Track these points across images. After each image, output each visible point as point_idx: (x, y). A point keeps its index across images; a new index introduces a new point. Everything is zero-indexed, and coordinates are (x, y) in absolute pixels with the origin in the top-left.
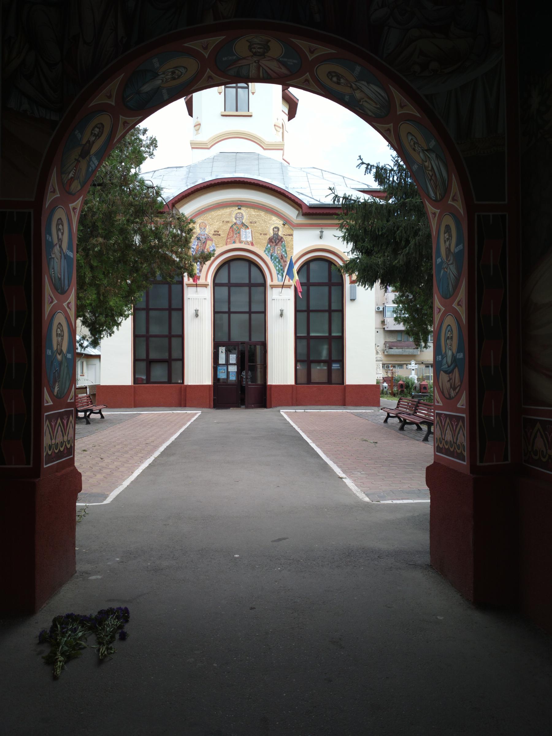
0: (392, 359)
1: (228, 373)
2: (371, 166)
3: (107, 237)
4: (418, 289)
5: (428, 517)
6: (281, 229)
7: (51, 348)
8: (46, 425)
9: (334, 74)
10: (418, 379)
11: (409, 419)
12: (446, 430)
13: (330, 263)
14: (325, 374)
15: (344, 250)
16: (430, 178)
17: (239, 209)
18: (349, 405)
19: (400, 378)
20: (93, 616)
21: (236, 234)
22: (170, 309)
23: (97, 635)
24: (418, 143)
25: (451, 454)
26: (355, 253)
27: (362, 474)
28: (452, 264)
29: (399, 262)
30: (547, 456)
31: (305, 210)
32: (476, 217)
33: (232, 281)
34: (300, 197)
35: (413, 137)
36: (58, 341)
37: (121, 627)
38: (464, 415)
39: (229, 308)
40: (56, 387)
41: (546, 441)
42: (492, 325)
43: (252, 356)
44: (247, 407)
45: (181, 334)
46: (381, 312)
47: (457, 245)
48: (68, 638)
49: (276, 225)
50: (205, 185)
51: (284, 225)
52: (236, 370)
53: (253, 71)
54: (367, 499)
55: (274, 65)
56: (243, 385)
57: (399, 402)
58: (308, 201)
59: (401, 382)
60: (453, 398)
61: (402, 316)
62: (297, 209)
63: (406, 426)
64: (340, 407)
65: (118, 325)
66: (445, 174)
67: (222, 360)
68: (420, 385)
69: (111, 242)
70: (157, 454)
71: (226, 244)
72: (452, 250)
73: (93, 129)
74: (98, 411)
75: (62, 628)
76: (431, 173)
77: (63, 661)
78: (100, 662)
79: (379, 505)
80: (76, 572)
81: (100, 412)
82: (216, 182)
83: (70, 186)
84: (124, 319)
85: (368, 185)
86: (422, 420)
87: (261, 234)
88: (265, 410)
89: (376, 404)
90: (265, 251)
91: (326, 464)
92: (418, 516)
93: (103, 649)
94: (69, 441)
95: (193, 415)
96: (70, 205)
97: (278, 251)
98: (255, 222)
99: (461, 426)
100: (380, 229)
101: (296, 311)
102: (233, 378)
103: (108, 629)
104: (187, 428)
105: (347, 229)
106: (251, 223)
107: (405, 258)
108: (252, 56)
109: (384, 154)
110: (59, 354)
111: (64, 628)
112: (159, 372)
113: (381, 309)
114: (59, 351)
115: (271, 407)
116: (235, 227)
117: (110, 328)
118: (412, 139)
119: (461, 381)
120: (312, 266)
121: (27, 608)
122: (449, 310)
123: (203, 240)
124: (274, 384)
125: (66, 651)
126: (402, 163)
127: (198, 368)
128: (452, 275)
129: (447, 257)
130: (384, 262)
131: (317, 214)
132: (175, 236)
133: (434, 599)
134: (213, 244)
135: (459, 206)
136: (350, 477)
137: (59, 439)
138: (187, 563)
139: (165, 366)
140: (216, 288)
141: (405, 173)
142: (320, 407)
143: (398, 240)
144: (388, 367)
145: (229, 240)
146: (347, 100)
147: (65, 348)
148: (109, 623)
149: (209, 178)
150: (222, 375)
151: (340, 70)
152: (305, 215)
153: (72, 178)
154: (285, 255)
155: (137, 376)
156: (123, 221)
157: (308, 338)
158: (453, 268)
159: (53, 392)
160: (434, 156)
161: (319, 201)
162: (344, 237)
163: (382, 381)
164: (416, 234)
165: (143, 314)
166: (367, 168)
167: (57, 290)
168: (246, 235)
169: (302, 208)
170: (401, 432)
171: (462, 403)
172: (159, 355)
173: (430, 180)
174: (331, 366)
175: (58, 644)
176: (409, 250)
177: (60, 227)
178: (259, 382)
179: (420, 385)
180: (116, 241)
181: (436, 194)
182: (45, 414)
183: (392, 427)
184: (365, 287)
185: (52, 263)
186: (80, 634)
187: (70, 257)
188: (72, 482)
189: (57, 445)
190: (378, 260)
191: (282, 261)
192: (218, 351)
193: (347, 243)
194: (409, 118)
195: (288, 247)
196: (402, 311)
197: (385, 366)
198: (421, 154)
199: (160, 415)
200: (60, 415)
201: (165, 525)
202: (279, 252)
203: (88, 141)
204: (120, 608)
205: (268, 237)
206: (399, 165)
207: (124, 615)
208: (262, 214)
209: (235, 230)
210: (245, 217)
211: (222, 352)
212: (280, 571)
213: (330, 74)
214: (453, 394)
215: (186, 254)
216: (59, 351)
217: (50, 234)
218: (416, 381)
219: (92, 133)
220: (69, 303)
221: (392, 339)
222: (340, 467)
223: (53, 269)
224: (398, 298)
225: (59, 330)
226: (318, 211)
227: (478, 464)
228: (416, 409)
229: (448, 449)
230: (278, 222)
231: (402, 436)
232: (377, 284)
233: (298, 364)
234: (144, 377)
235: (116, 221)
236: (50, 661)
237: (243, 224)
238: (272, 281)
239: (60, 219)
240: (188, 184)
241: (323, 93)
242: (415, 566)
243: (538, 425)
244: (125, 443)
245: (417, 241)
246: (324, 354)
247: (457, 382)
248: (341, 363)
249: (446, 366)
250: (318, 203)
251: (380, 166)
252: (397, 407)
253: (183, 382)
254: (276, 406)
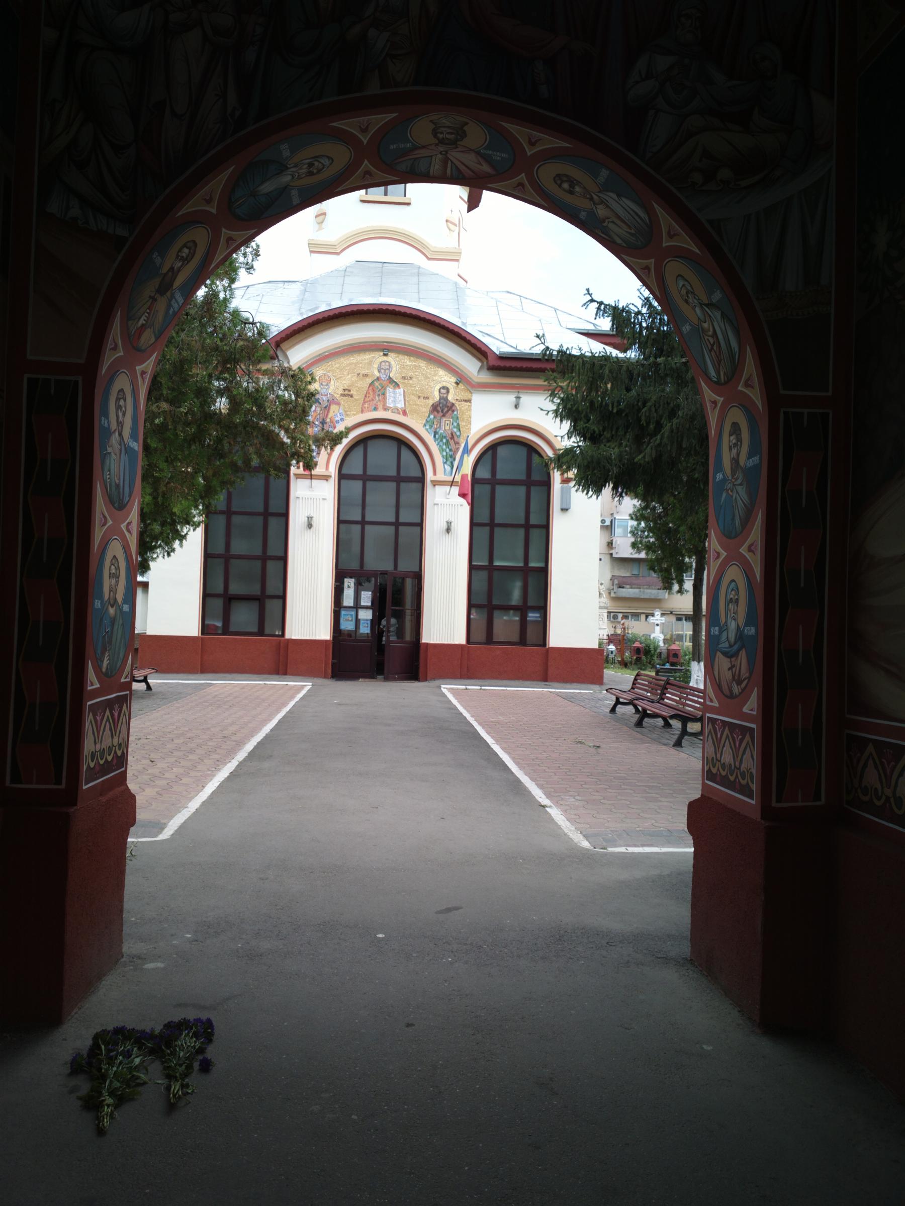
0: (623, 604)
1: (357, 621)
2: (606, 306)
3: (174, 402)
4: (672, 499)
5: (689, 879)
6: (452, 391)
7: (101, 597)
8: (89, 721)
9: (565, 179)
10: (665, 641)
11: (651, 708)
12: (724, 746)
13: (531, 449)
14: (517, 628)
15: (558, 434)
16: (710, 347)
17: (385, 355)
18: (552, 681)
19: (635, 639)
20: (157, 1032)
21: (379, 395)
22: (266, 514)
23: (163, 1063)
24: (693, 293)
25: (731, 785)
26: (573, 439)
27: (577, 800)
28: (741, 484)
29: (644, 457)
30: (884, 798)
31: (493, 362)
32: (782, 415)
33: (369, 472)
34: (486, 340)
35: (686, 283)
36: (111, 585)
37: (201, 1051)
38: (754, 726)
39: (363, 516)
40: (106, 659)
41: (881, 772)
42: (802, 585)
43: (399, 592)
44: (387, 679)
45: (283, 554)
46: (608, 528)
47: (750, 457)
48: (118, 1068)
49: (444, 384)
50: (331, 314)
51: (457, 384)
52: (370, 617)
53: (437, 167)
54: (585, 844)
55: (470, 160)
56: (381, 642)
57: (635, 679)
58: (497, 347)
59: (637, 645)
60: (736, 696)
61: (645, 540)
62: (480, 360)
63: (646, 720)
64: (540, 683)
65: (182, 538)
66: (734, 344)
67: (348, 599)
68: (668, 650)
69: (182, 410)
70: (242, 755)
71: (362, 412)
72: (742, 463)
73: (180, 251)
74: (142, 678)
75: (109, 1051)
76: (712, 340)
77: (112, 1105)
78: (171, 1107)
79: (606, 854)
80: (122, 956)
81: (145, 680)
82: (349, 310)
83: (139, 338)
84: (192, 528)
85: (594, 325)
86: (673, 712)
87: (419, 397)
88: (416, 684)
89: (597, 679)
90: (425, 425)
91: (518, 781)
92: (668, 875)
93: (176, 1087)
94: (120, 745)
95: (301, 688)
96: (138, 368)
97: (446, 426)
98: (411, 378)
99: (748, 743)
100: (615, 404)
101: (473, 524)
102: (365, 629)
103: (182, 1054)
104: (290, 712)
105: (562, 399)
106: (404, 378)
107: (654, 452)
108: (437, 145)
109: (627, 289)
110: (112, 606)
111: (112, 1051)
112: (244, 616)
113: (608, 523)
114: (112, 602)
115: (425, 680)
116: (377, 384)
117: (168, 542)
118: (683, 285)
119: (751, 673)
120: (502, 451)
121: (48, 1014)
122: (734, 557)
123: (325, 404)
124: (432, 642)
125: (117, 1089)
126: (655, 304)
127: (309, 615)
128: (740, 502)
129: (733, 472)
130: (620, 457)
131: (514, 369)
132: (285, 403)
133: (700, 1017)
134: (341, 411)
135: (756, 396)
136: (557, 804)
137: (107, 742)
138: (301, 945)
139: (255, 606)
140: (343, 481)
141: (660, 319)
142: (505, 682)
143: (643, 422)
144: (615, 617)
145: (366, 405)
146: (583, 218)
147: (120, 597)
148: (181, 1044)
149: (337, 303)
150: (347, 625)
151: (575, 173)
152: (492, 369)
153: (143, 325)
154: (458, 433)
155: (207, 622)
156: (203, 377)
157: (491, 569)
158: (742, 490)
159: (100, 668)
160: (718, 314)
161: (516, 348)
162: (556, 411)
163: (605, 641)
164: (673, 414)
165: (221, 520)
166: (599, 309)
167: (112, 503)
168: (395, 398)
169: (487, 359)
170: (639, 729)
171: (751, 706)
172: (245, 590)
173: (710, 351)
174: (526, 616)
175: (104, 1077)
176: (661, 439)
177: (122, 403)
178: (408, 637)
179: (668, 650)
180: (190, 410)
181: (718, 373)
182: (89, 703)
183: (622, 720)
184: (587, 493)
185: (108, 461)
186: (137, 1061)
187: (132, 449)
188: (121, 810)
189: (103, 752)
190: (612, 451)
191: (452, 442)
192: (343, 583)
193: (561, 421)
194: (681, 254)
195: (463, 420)
196: (644, 532)
197: (612, 616)
198: (698, 310)
199: (243, 687)
200: (109, 704)
201: (262, 879)
202: (447, 428)
203: (172, 268)
204: (198, 1020)
205: (431, 402)
206: (651, 306)
207: (205, 1030)
208: (423, 364)
209: (378, 388)
210: (394, 369)
211: (349, 587)
212: (451, 963)
213: (559, 178)
214: (736, 690)
215: (302, 434)
216: (112, 602)
217: (107, 416)
218: (661, 644)
219: (178, 256)
220: (129, 524)
221: (623, 573)
222: (540, 786)
223: (109, 470)
224: (638, 510)
225: (113, 567)
226: (513, 364)
227: (774, 804)
228: (663, 694)
229: (726, 777)
230: (448, 379)
231: (639, 736)
232: (607, 491)
233: (473, 611)
234: (219, 624)
235: (192, 376)
236: (92, 1104)
237: (391, 380)
238: (435, 473)
239: (122, 390)
240: (303, 311)
241: (543, 203)
242: (666, 960)
243: (871, 748)
244: (189, 735)
245: (674, 426)
246: (516, 597)
247: (745, 673)
248: (542, 611)
249: (727, 645)
250: (514, 351)
251: (620, 306)
252: (633, 688)
253: (283, 635)
254: (434, 679)
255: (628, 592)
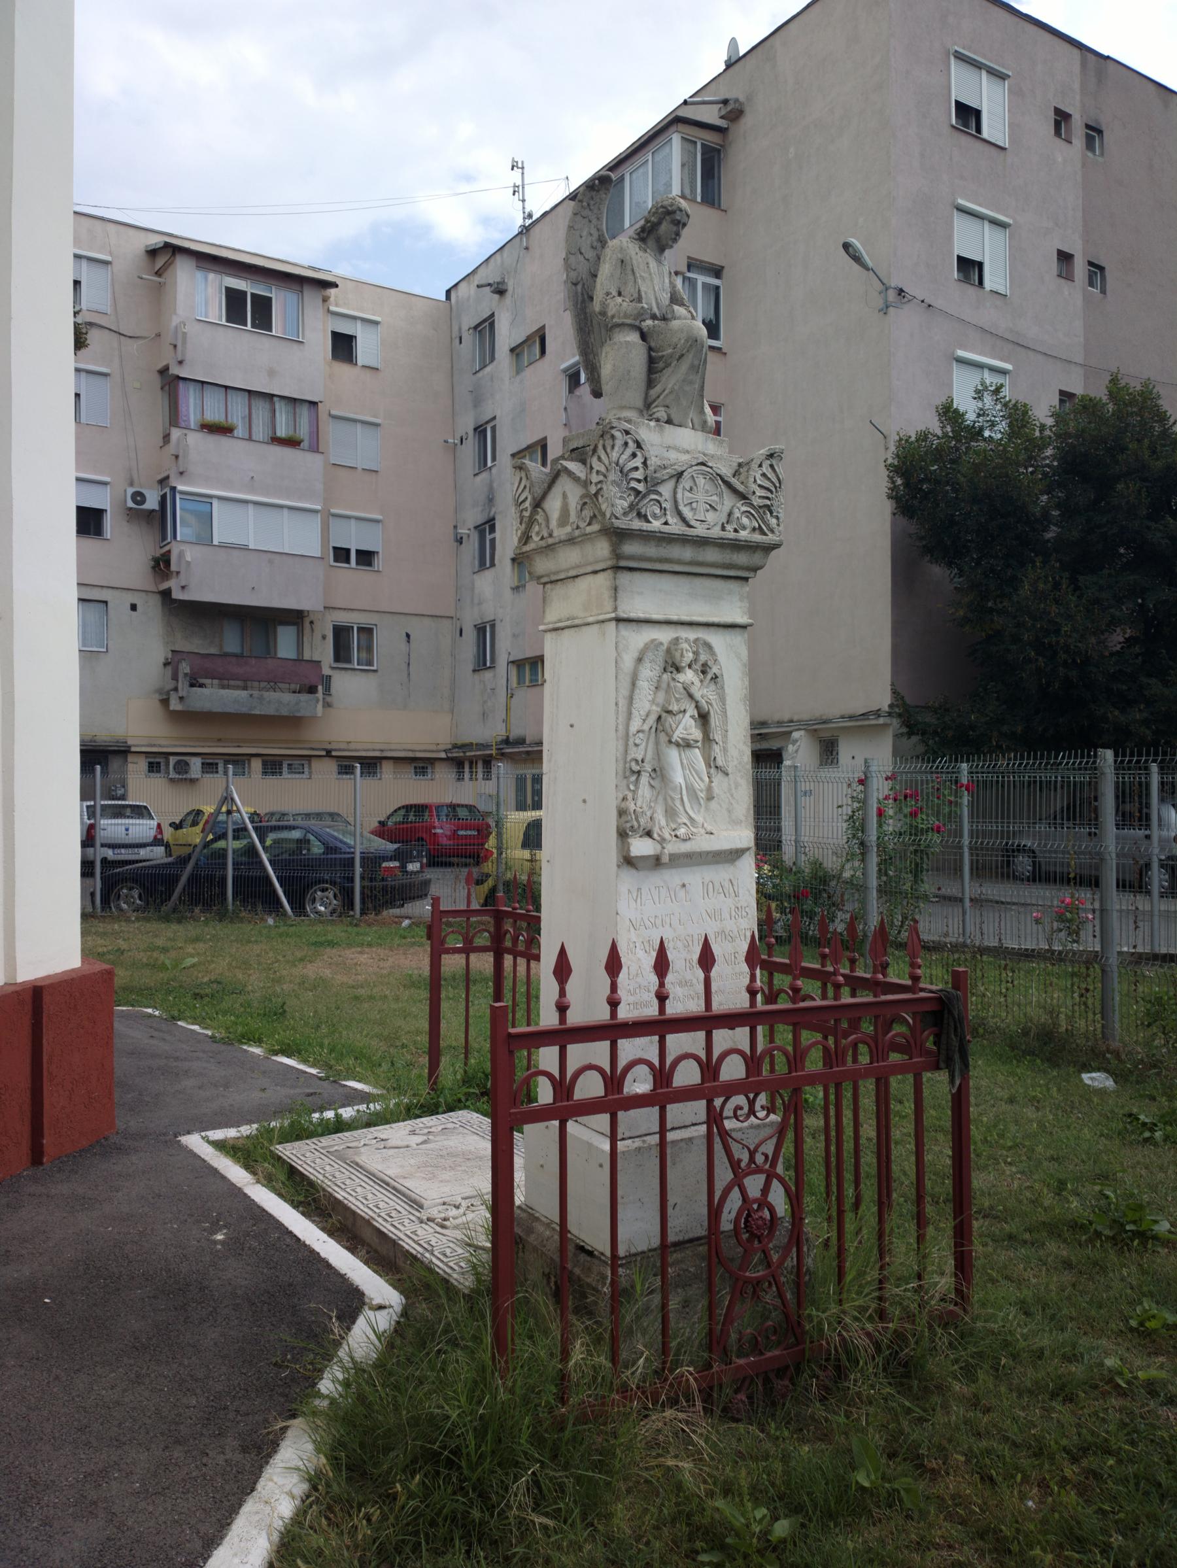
41: (832, 1097)
113: (152, 503)
221: (196, 644)
255: (213, 697)
